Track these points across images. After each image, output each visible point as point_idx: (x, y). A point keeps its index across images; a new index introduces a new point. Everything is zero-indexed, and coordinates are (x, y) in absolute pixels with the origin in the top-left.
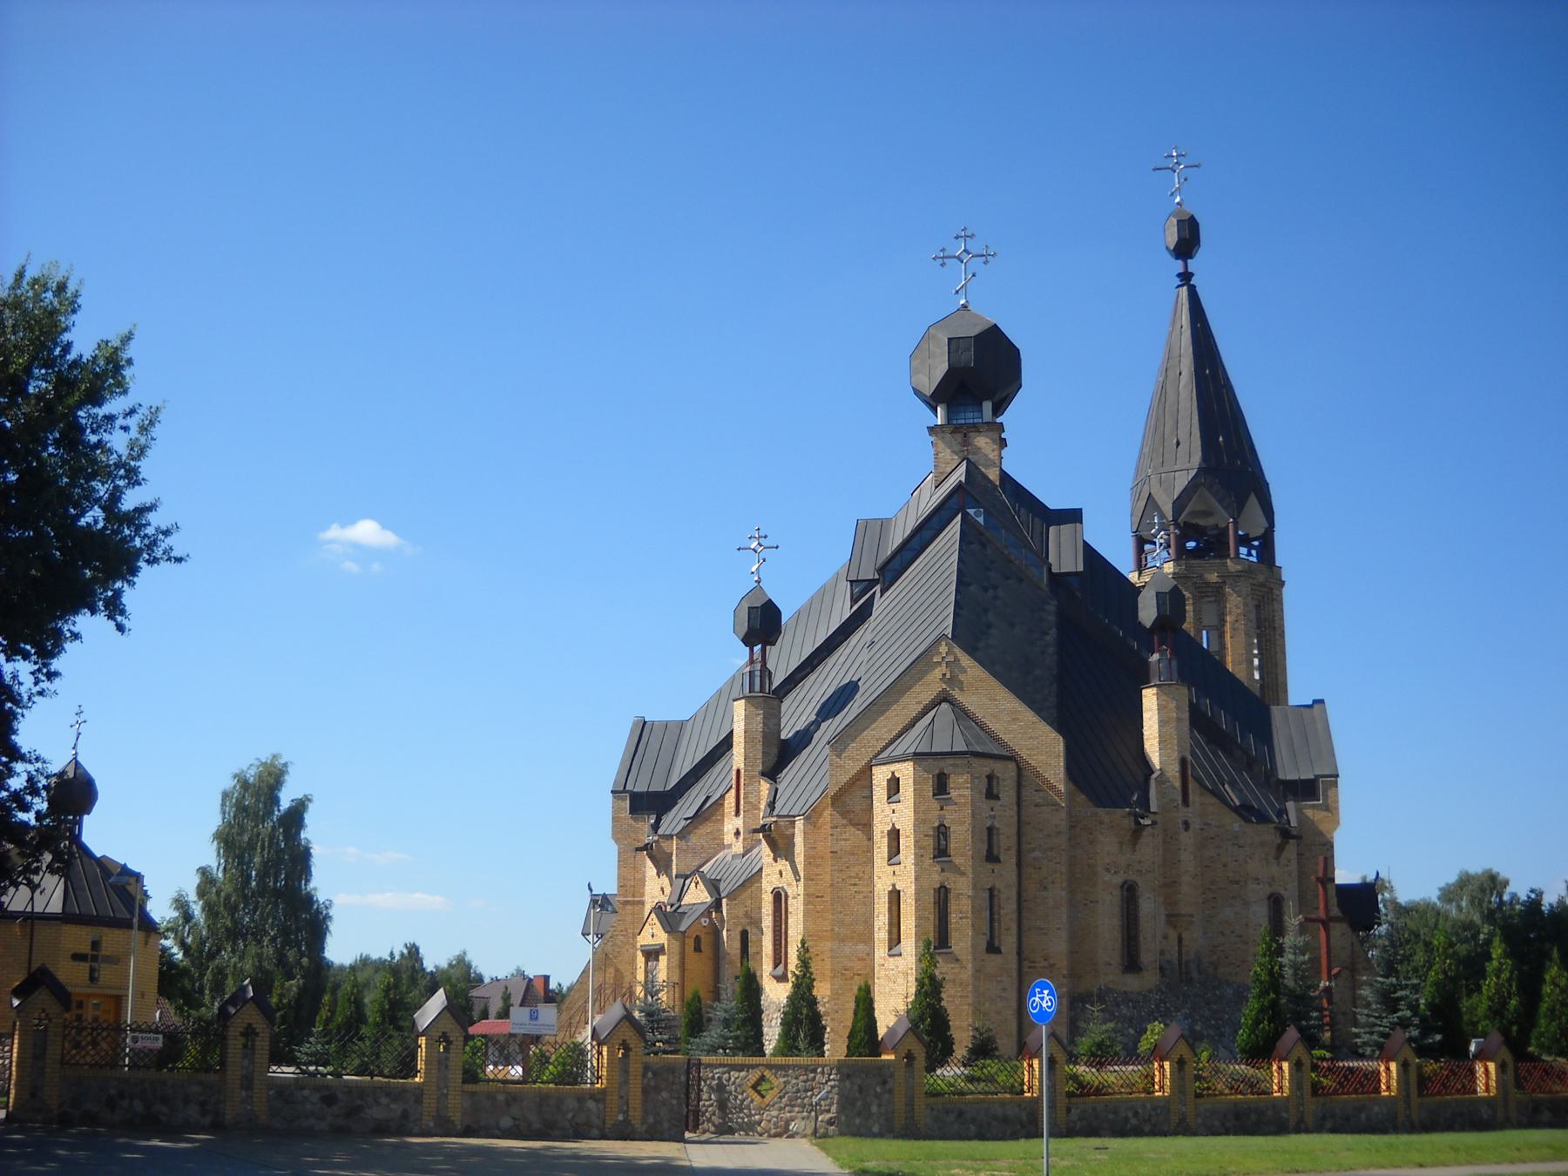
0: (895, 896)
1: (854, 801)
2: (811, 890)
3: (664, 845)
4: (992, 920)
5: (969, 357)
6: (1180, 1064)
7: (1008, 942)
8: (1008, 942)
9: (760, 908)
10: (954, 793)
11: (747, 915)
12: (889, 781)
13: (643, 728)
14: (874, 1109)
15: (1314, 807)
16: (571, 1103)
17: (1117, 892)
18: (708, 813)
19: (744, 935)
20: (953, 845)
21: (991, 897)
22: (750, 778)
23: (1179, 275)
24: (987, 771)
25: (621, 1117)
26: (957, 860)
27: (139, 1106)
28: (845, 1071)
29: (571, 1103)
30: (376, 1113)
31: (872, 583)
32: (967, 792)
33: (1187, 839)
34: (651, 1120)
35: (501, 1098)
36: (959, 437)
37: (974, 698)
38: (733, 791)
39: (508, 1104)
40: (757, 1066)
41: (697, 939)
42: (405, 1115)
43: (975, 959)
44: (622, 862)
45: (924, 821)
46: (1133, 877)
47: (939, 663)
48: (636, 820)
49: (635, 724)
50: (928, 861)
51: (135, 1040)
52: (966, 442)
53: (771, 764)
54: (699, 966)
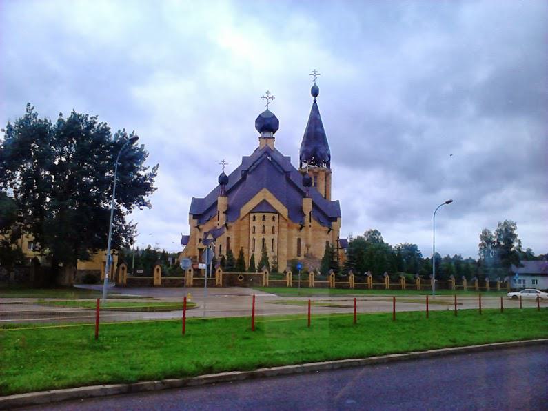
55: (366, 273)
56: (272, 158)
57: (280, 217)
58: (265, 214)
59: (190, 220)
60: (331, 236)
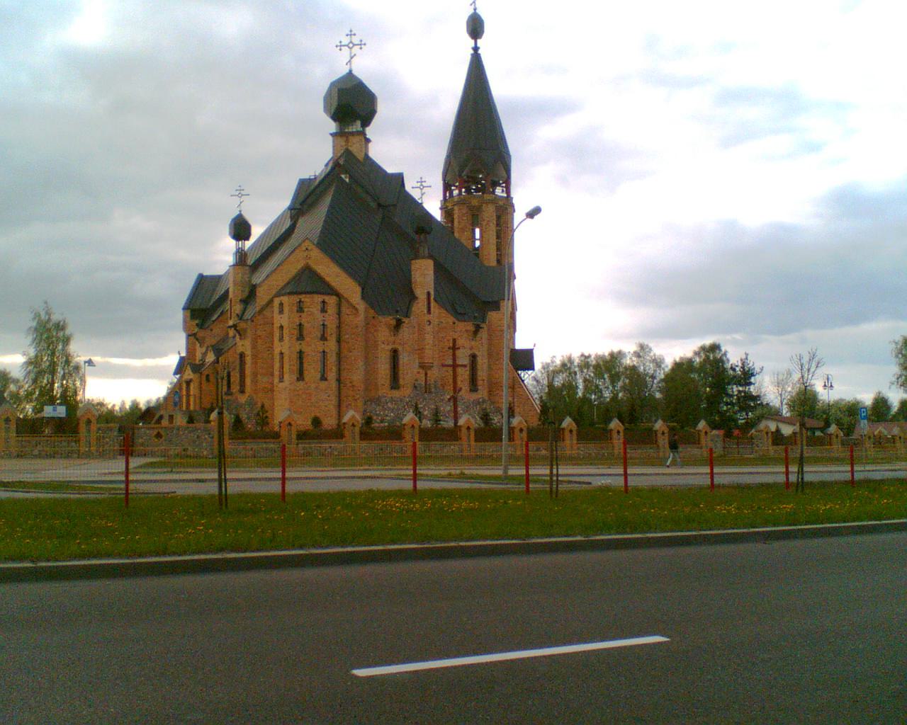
8: (332, 375)
12: (280, 304)
17: (388, 353)
24: (321, 300)
33: (428, 329)
46: (396, 346)
55: (658, 395)
56: (351, 177)
57: (344, 304)
58: (303, 297)
59: (185, 321)
60: (485, 341)
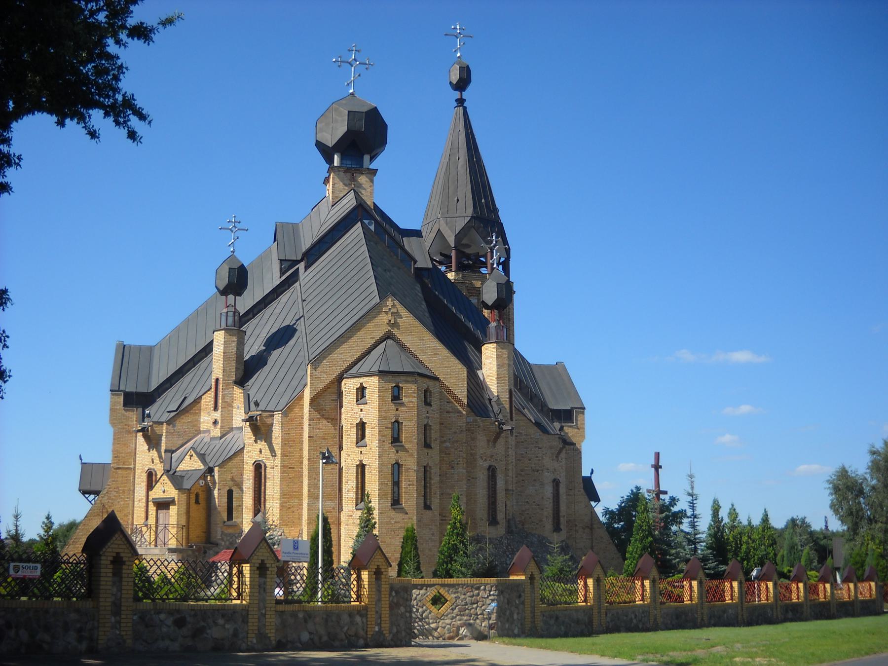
0: (361, 468)
1: (328, 403)
2: (286, 463)
3: (157, 429)
4: (425, 487)
5: (361, 125)
6: (598, 582)
7: (435, 502)
9: (242, 475)
10: (404, 400)
11: (232, 479)
13: (123, 351)
14: (515, 616)
15: (570, 426)
16: (345, 618)
17: (486, 473)
18: (187, 409)
19: (230, 493)
20: (403, 437)
21: (425, 471)
22: (226, 385)
23: (456, 100)
25: (377, 629)
26: (407, 446)
27: (24, 635)
28: (500, 588)
29: (345, 618)
30: (215, 633)
31: (298, 262)
32: (415, 400)
34: (395, 630)
35: (301, 615)
36: (349, 175)
37: (409, 338)
38: (212, 393)
39: (306, 621)
40: (434, 585)
41: (197, 495)
42: (236, 634)
43: (418, 513)
44: (117, 439)
45: (385, 418)
47: (387, 313)
48: (126, 411)
49: (118, 346)
50: (388, 445)
51: (17, 569)
52: (353, 179)
53: (240, 376)
54: (198, 513)
